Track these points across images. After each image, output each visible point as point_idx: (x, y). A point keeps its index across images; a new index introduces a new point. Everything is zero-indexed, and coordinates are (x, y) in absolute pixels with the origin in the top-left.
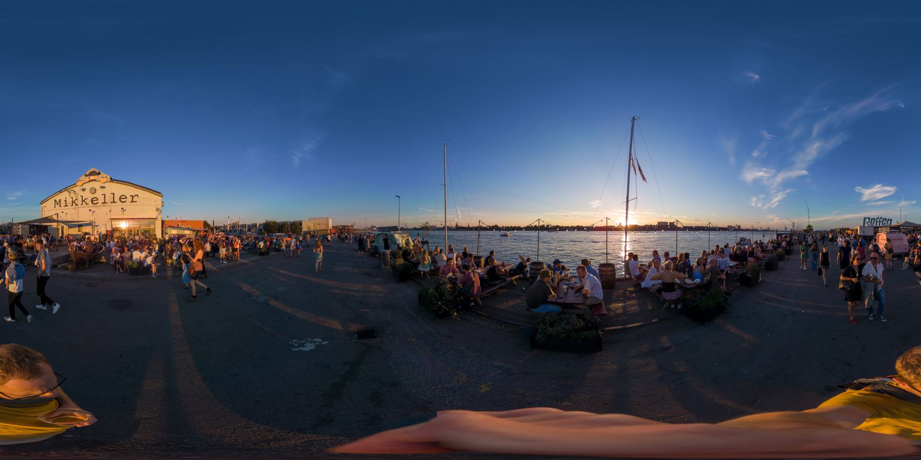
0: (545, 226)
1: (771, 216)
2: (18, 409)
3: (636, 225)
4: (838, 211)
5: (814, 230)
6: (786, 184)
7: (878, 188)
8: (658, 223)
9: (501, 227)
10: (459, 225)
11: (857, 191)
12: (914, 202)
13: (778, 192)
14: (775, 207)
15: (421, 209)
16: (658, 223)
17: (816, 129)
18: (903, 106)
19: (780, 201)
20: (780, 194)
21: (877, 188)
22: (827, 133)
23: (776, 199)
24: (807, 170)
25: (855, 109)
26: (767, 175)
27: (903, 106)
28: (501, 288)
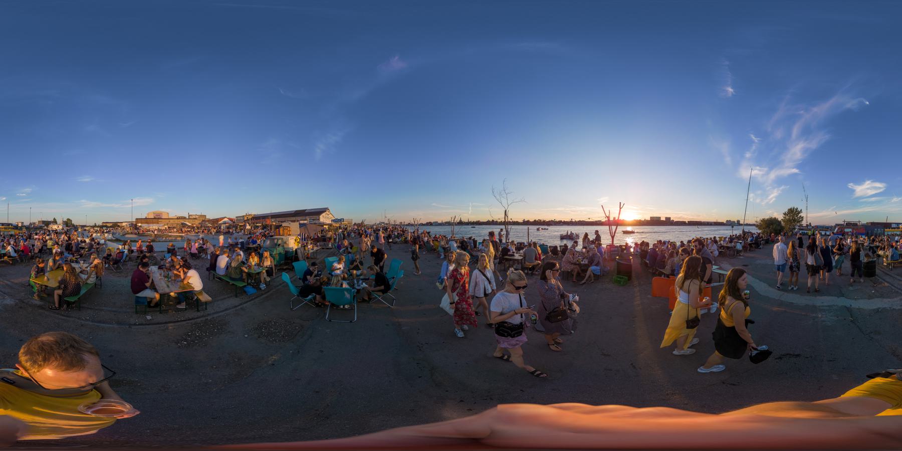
2: (50, 398)
3: (640, 220)
4: (834, 207)
6: (780, 181)
7: (868, 184)
8: (651, 217)
10: (463, 220)
11: (850, 187)
12: (4, 199)
13: (774, 188)
15: (434, 204)
16: (651, 217)
17: (795, 131)
18: (868, 103)
19: (776, 197)
20: (776, 190)
21: (868, 184)
22: (806, 132)
25: (822, 109)
26: (761, 173)
27: (868, 103)
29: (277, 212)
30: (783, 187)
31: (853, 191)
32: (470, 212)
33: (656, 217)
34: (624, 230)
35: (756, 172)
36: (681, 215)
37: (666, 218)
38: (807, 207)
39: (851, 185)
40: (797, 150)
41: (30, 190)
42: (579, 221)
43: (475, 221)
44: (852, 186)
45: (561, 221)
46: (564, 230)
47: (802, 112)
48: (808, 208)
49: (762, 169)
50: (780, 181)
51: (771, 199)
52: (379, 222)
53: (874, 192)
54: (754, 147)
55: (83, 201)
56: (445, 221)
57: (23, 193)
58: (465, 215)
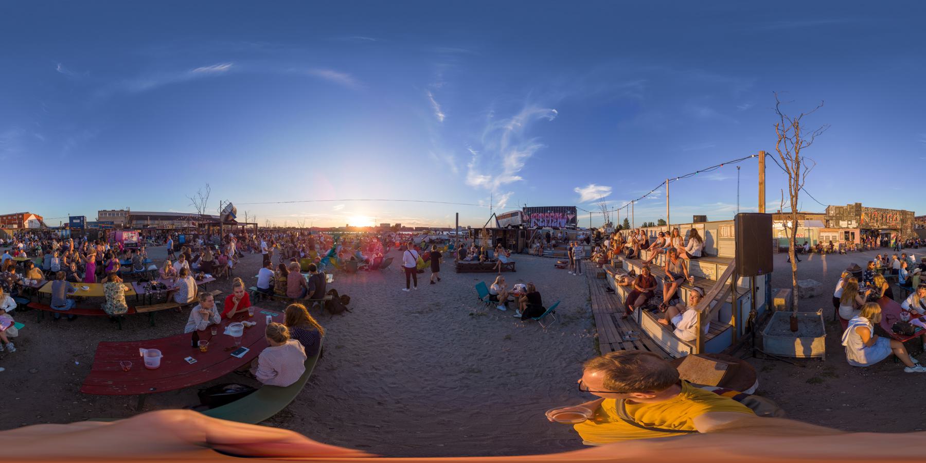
3: (370, 227)
11: (576, 191)
22: (515, 141)
30: (509, 194)
33: (386, 224)
36: (414, 221)
39: (577, 190)
45: (295, 228)
50: (504, 188)
51: (502, 205)
54: (474, 159)
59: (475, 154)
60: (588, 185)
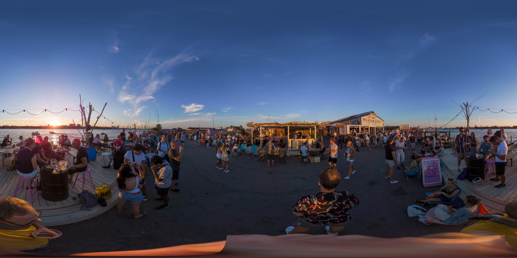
0: (76, 125)
1: (136, 121)
4: (173, 118)
5: (162, 129)
6: (142, 103)
9: (69, 125)
11: (182, 107)
12: (215, 114)
13: (138, 107)
14: (138, 116)
17: (154, 74)
18: (198, 59)
19: (140, 113)
20: (139, 109)
21: (193, 105)
22: (160, 75)
23: (138, 111)
24: (153, 96)
25: (172, 62)
26: (131, 99)
27: (198, 59)
28: (68, 157)
29: (337, 120)
30: (144, 107)
31: (184, 109)
32: (480, 122)
34: (51, 131)
35: (128, 98)
37: (78, 124)
38: (158, 120)
39: (183, 106)
40: (154, 85)
41: (230, 108)
42: (26, 126)
43: (25, 126)
44: (183, 107)
46: (35, 131)
47: (158, 63)
48: (159, 120)
49: (132, 96)
52: (428, 127)
53: (197, 110)
54: (128, 83)
55: (260, 115)
56: (412, 127)
57: (225, 111)
58: (477, 123)
59: (130, 79)
60: (191, 104)
